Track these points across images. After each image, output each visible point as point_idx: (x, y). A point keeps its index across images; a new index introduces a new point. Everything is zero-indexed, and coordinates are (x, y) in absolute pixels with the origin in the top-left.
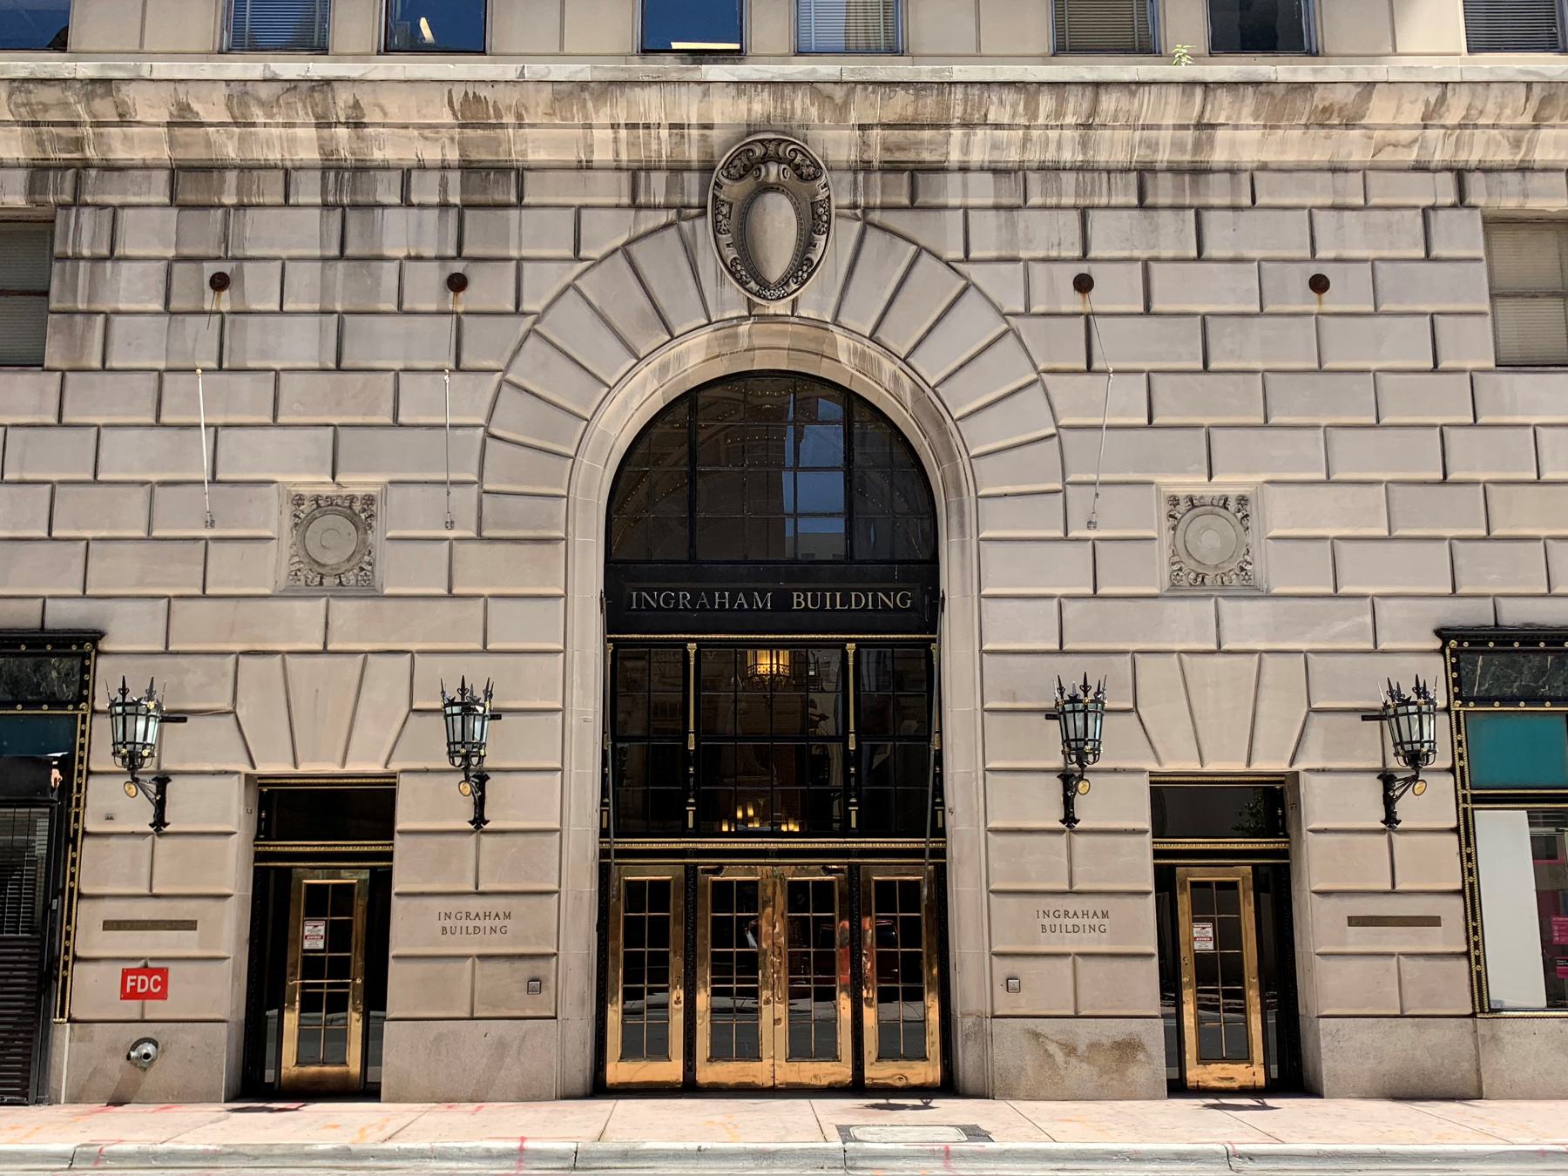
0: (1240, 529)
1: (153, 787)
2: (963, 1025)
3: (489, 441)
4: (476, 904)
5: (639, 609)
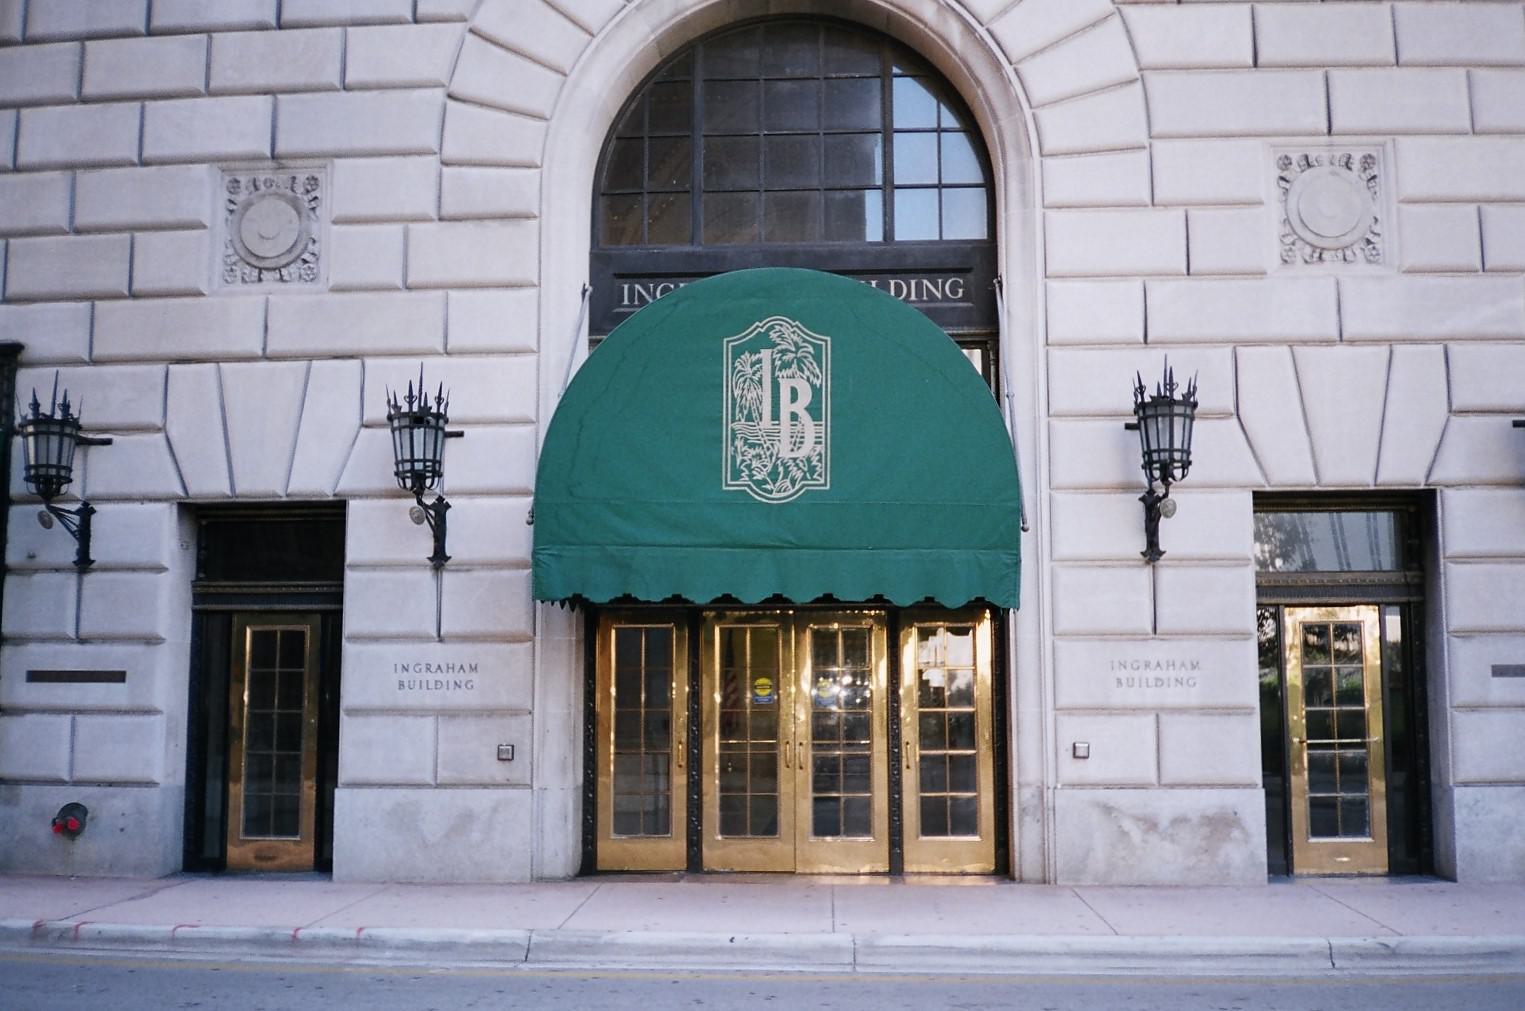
0: (1369, 194)
1: (76, 519)
3: (451, 104)
4: (437, 652)
5: (631, 305)
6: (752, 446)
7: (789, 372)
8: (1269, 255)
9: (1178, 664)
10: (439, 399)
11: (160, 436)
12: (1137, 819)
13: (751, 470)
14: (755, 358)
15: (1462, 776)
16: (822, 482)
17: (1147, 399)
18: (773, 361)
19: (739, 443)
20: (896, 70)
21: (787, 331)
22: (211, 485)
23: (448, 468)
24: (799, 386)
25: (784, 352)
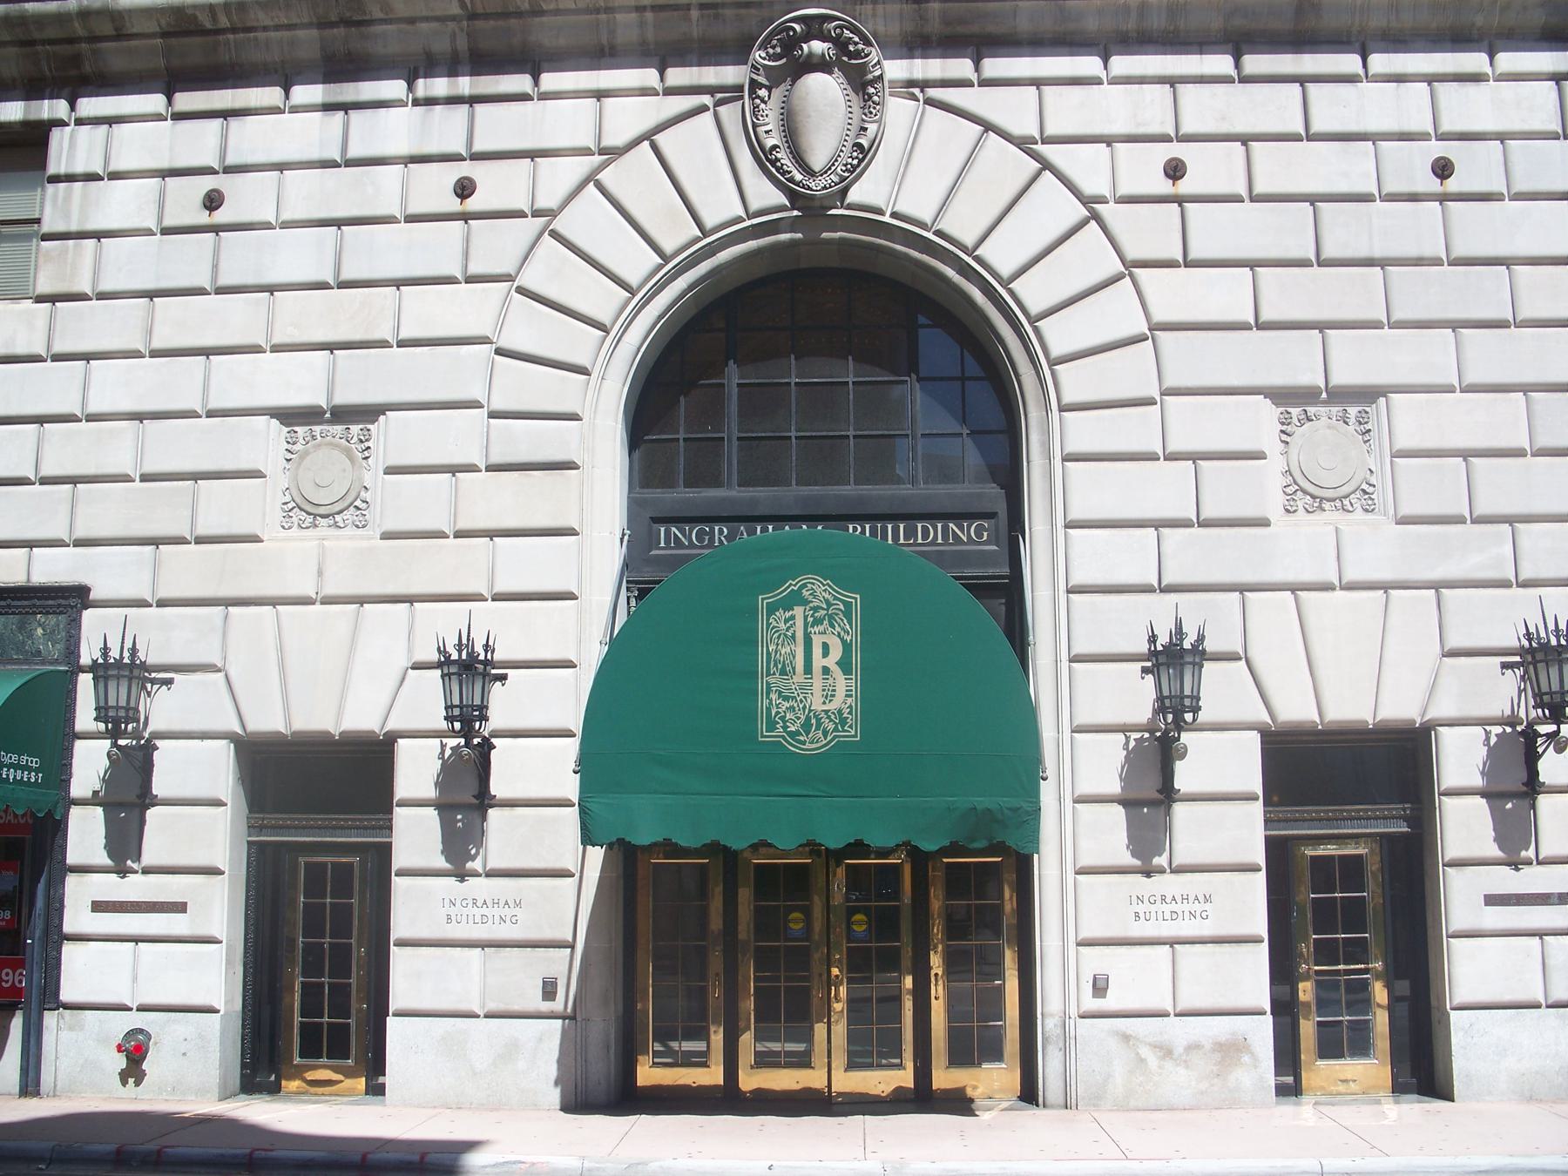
2: (1047, 1024)
5: (668, 546)
6: (786, 699)
7: (821, 628)
8: (1272, 505)
9: (1191, 899)
10: (486, 647)
11: (221, 675)
12: (1156, 1046)
13: (785, 722)
14: (788, 614)
15: (1457, 1001)
16: (852, 733)
17: (1160, 648)
18: (806, 618)
19: (774, 696)
20: (922, 320)
21: (820, 590)
22: (267, 719)
23: (492, 713)
24: (829, 647)
25: (816, 609)
